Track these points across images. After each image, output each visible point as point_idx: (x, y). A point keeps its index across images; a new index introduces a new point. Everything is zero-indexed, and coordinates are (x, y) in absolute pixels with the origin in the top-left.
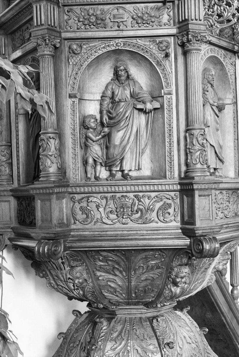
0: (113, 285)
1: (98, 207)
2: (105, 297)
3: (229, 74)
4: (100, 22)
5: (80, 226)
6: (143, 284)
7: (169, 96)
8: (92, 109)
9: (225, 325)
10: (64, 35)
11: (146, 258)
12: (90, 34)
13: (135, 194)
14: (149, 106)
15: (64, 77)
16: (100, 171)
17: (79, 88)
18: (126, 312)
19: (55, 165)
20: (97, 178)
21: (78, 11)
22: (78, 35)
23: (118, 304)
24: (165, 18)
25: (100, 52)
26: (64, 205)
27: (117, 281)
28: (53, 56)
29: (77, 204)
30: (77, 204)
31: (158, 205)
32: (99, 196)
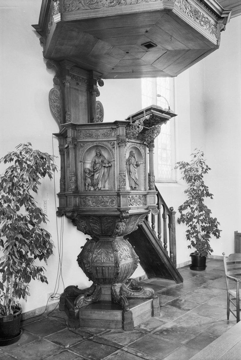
0: (96, 228)
1: (89, 200)
2: (94, 233)
3: (142, 153)
4: (91, 136)
5: (83, 207)
6: (106, 228)
7: (114, 162)
8: (88, 166)
9: (154, 248)
10: (78, 140)
11: (106, 219)
12: (87, 140)
13: (132, 196)
14: (107, 165)
15: (78, 155)
16: (91, 188)
17: (83, 159)
18: (102, 239)
19: (74, 186)
20: (90, 190)
21: (84, 132)
22: (83, 140)
23: (99, 235)
24: (113, 134)
25: (91, 146)
26: (77, 200)
27: (97, 227)
28: (74, 148)
29: (82, 199)
30: (82, 199)
31: (110, 200)
32: (89, 197)
